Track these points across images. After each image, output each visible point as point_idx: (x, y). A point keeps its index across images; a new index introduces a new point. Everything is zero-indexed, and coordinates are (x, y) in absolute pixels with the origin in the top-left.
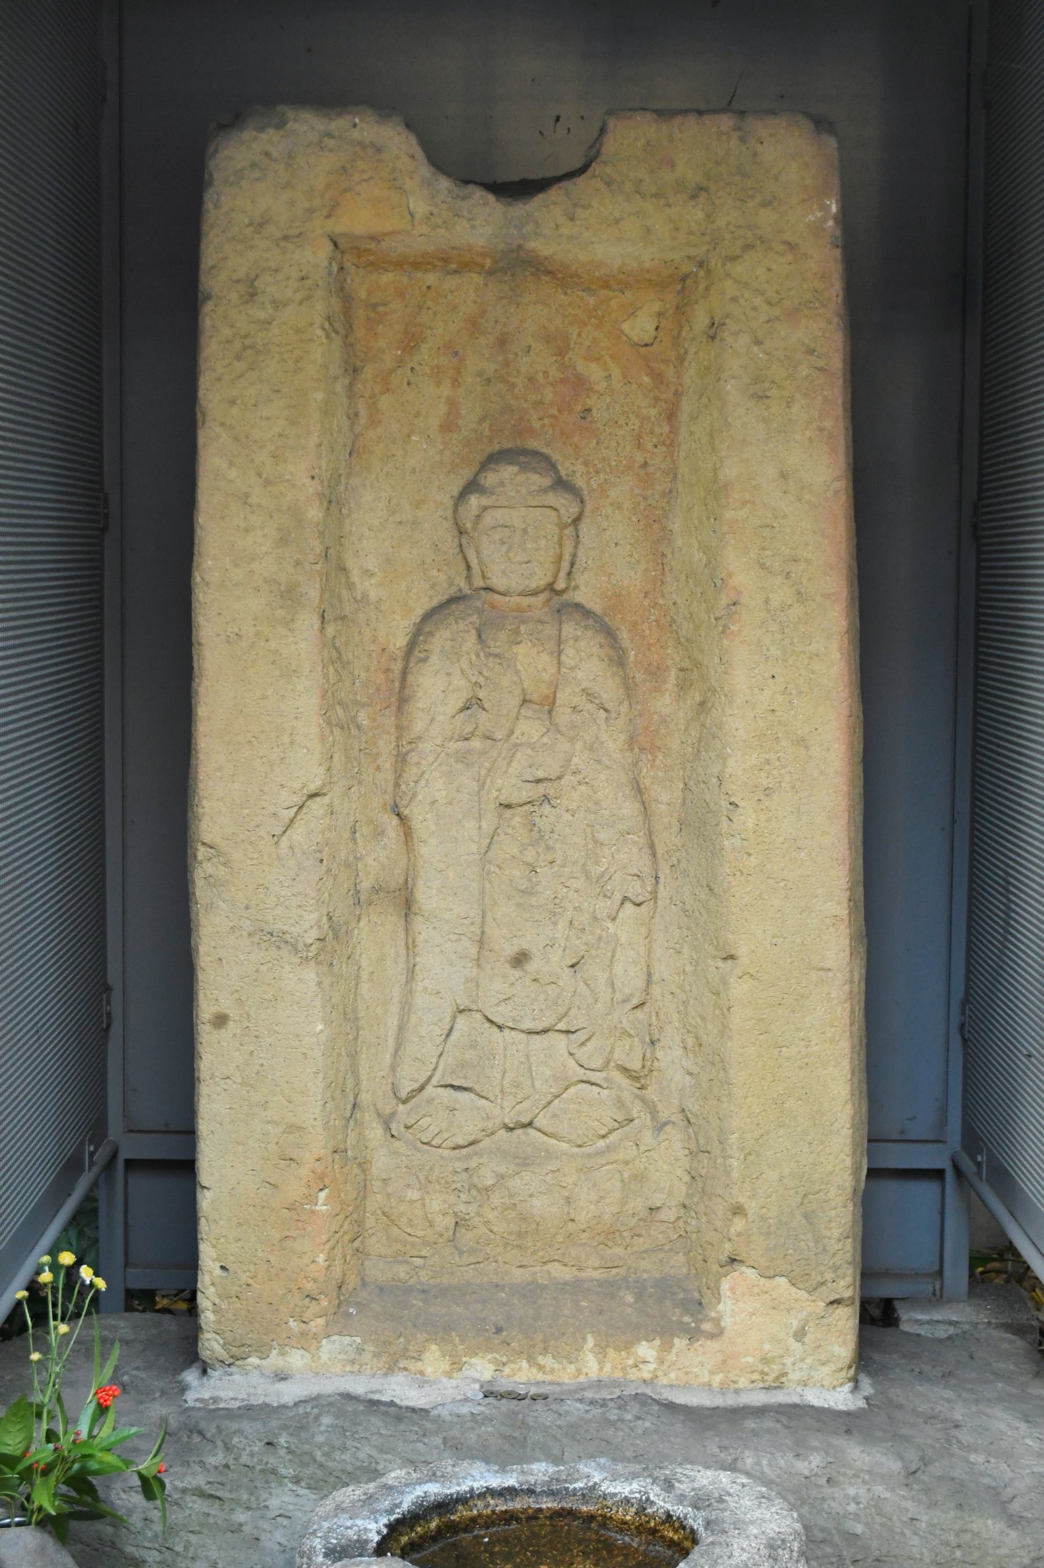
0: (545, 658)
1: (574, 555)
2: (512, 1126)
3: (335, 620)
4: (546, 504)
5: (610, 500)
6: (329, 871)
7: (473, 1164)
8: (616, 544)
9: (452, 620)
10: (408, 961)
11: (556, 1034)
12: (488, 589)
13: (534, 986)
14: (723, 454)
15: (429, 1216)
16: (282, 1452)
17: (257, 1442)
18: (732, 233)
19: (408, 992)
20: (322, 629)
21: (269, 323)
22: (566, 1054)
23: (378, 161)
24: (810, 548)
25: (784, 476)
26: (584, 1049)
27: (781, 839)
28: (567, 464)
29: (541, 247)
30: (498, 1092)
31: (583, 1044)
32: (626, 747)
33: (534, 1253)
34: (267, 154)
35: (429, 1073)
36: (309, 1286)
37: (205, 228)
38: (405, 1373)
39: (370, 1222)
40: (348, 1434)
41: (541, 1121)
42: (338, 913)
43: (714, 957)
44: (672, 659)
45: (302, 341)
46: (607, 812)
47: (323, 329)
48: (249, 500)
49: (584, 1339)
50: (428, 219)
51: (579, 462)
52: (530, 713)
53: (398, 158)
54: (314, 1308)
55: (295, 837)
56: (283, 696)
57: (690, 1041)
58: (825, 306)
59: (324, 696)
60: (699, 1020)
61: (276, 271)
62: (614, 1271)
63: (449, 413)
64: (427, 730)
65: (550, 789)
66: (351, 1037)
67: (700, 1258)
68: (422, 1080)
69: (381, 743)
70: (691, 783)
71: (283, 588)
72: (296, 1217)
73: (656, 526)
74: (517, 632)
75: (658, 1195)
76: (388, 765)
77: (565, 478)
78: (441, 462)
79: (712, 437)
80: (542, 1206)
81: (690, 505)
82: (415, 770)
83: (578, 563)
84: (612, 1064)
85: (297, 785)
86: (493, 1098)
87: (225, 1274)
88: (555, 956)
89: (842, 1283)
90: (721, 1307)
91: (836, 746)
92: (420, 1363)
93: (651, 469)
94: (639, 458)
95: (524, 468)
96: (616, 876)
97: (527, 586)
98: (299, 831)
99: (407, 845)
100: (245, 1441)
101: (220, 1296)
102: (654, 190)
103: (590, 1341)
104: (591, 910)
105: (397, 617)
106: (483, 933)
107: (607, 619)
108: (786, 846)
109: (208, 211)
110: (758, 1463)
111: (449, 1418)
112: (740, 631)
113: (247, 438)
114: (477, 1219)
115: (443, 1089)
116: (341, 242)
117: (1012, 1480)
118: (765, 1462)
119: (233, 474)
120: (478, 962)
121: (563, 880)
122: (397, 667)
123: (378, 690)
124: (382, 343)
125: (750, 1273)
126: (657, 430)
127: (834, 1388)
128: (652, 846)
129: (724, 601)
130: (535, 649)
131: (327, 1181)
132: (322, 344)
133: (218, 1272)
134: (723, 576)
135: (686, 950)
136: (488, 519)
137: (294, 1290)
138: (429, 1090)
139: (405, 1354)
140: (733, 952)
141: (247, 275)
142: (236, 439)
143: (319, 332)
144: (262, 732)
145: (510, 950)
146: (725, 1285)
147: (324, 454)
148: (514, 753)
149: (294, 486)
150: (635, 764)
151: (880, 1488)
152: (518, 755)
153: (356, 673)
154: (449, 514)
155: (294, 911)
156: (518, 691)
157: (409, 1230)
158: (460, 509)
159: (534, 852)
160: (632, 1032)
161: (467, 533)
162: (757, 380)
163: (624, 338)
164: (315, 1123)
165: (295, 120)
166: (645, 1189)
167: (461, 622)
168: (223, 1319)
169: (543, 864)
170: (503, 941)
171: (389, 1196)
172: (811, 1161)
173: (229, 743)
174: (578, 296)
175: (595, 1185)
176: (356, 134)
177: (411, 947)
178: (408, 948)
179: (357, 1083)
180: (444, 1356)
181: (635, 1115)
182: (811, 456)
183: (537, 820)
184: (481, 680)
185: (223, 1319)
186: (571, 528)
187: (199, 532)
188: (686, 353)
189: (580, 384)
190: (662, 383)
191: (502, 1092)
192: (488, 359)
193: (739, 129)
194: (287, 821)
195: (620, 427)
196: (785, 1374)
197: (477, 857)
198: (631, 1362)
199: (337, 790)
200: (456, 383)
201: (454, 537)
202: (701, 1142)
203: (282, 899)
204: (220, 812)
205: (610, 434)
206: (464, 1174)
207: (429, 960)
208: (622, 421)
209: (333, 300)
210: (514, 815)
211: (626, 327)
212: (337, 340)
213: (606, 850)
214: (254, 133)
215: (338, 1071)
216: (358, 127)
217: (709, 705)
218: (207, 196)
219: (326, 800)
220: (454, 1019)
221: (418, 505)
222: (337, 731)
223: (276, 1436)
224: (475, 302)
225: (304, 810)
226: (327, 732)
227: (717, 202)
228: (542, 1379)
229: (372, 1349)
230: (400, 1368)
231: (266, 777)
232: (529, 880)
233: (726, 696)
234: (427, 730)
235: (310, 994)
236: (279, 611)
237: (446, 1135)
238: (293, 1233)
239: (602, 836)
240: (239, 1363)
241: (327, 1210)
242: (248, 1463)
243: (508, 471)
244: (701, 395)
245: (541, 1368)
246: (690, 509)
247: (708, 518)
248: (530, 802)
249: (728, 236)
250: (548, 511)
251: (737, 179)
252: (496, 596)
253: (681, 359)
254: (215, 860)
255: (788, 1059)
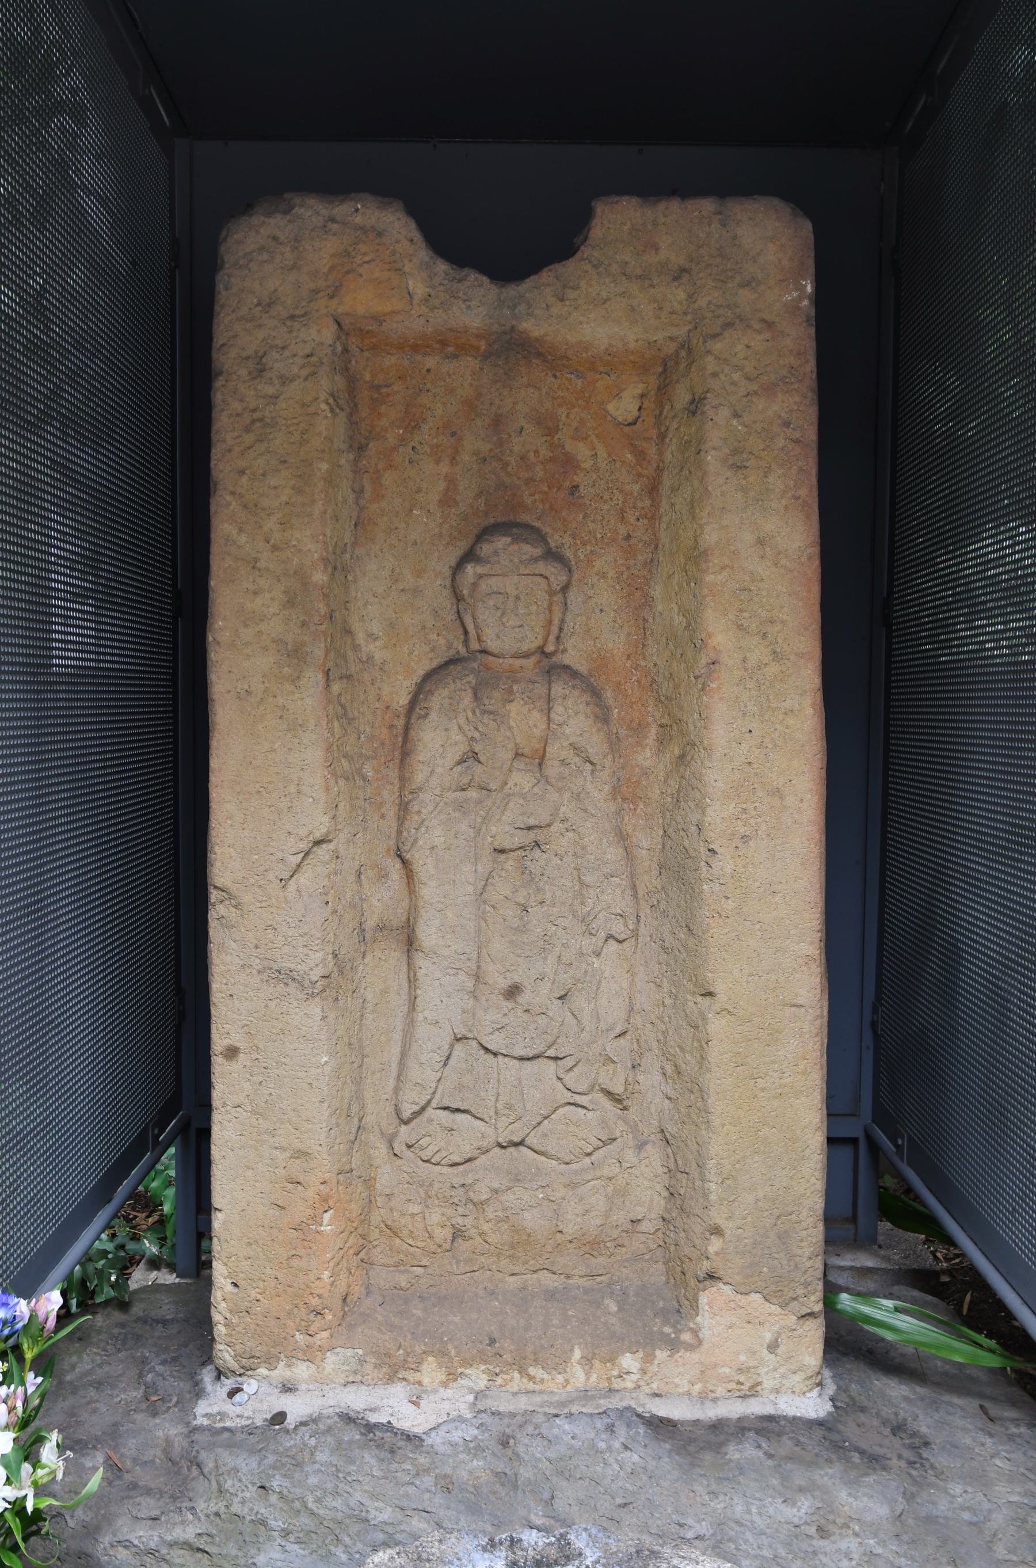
0: (536, 714)
1: (563, 621)
2: (505, 1144)
3: (341, 678)
4: (537, 572)
5: (595, 570)
6: (334, 912)
7: (469, 1181)
8: (601, 610)
9: (450, 679)
10: (410, 993)
11: (546, 1060)
12: (484, 652)
13: (525, 1017)
14: (704, 521)
15: (429, 1228)
16: (274, 1498)
17: (250, 1486)
18: (713, 312)
19: (410, 1023)
20: (328, 686)
21: (277, 398)
22: (555, 1078)
23: (379, 245)
24: (786, 609)
25: (761, 542)
26: (571, 1074)
27: (757, 884)
28: (556, 537)
29: (532, 327)
30: (492, 1112)
31: (570, 1069)
32: (610, 797)
33: (525, 1263)
34: (275, 238)
35: (429, 1097)
36: (314, 1302)
37: (217, 308)
38: (404, 1383)
39: (375, 1234)
40: (341, 1475)
41: (530, 1141)
42: (343, 951)
43: (693, 993)
44: (653, 716)
45: (307, 415)
46: (592, 857)
47: (328, 404)
48: (258, 565)
49: (572, 1350)
50: (427, 300)
51: (566, 536)
52: (522, 766)
53: (398, 242)
54: (318, 1323)
55: (302, 880)
56: (290, 749)
57: (669, 1069)
58: (800, 381)
59: (328, 749)
60: (677, 1049)
61: (283, 348)
62: (599, 1279)
63: (447, 489)
64: (427, 781)
65: (540, 835)
66: (356, 1065)
67: (679, 1269)
68: (423, 1103)
69: (385, 793)
70: (671, 831)
71: (290, 647)
72: (303, 1237)
73: (638, 594)
74: (510, 691)
75: (639, 1208)
76: (392, 813)
77: (554, 550)
78: (441, 535)
79: (693, 507)
80: (530, 1219)
81: (671, 572)
82: (416, 817)
83: (565, 628)
84: (597, 1087)
85: (303, 832)
86: (487, 1119)
87: (236, 1290)
88: (545, 988)
89: (813, 1298)
90: (699, 1319)
91: (809, 796)
92: (418, 1374)
93: (633, 541)
94: (623, 531)
95: (516, 540)
96: (601, 915)
97: (519, 648)
98: (306, 875)
99: (409, 887)
100: (238, 1484)
101: (231, 1311)
102: (639, 272)
103: (577, 1354)
104: (578, 946)
105: (400, 677)
106: (479, 967)
107: (592, 680)
108: (762, 890)
109: (219, 293)
110: (748, 1512)
111: (441, 1449)
112: (719, 688)
113: (256, 506)
114: (473, 1231)
115: (441, 1111)
116: (346, 322)
117: (990, 1511)
118: (754, 1510)
119: (243, 539)
120: (474, 995)
121: (551, 918)
122: (400, 723)
123: (382, 744)
124: (384, 422)
125: (727, 1289)
126: (639, 504)
127: (804, 1393)
128: (634, 887)
129: (704, 661)
130: (527, 707)
131: (331, 1203)
132: (327, 417)
133: (230, 1288)
134: (703, 636)
135: (665, 984)
136: (484, 587)
137: (301, 1305)
138: (430, 1112)
139: (404, 1365)
140: (712, 989)
141: (256, 352)
142: (245, 507)
143: (323, 406)
144: (270, 782)
145: (503, 983)
146: (704, 1299)
147: (329, 522)
148: (508, 803)
149: (300, 551)
150: (618, 812)
151: (872, 1542)
152: (511, 804)
153: (362, 728)
154: (448, 582)
155: (301, 950)
156: (511, 746)
157: (410, 1241)
158: (457, 577)
159: (525, 893)
160: (615, 1059)
161: (464, 600)
162: (736, 451)
163: (609, 418)
164: (319, 1148)
165: (301, 206)
166: (627, 1203)
167: (458, 682)
168: (234, 1333)
169: (533, 904)
170: (497, 974)
171: (391, 1210)
172: (785, 1185)
173: (239, 793)
174: (567, 378)
175: (581, 1199)
176: (358, 219)
177: (412, 981)
178: (410, 982)
179: (363, 1107)
180: (440, 1368)
181: (618, 1135)
182: (787, 523)
183: (528, 863)
184: (477, 735)
185: (234, 1333)
186: (560, 595)
187: (212, 595)
188: (667, 429)
189: (569, 462)
190: (644, 459)
191: (496, 1113)
192: (483, 439)
193: (720, 213)
194: (294, 866)
195: (606, 502)
196: (759, 1384)
197: (473, 898)
198: (615, 1373)
199: (342, 837)
200: (453, 461)
201: (452, 604)
202: (680, 1163)
203: (290, 939)
204: (231, 857)
205: (596, 508)
206: (462, 1189)
207: (430, 995)
208: (606, 496)
209: (337, 378)
210: (507, 859)
211: (610, 407)
212: (342, 418)
213: (591, 891)
214: (262, 218)
215: (342, 1099)
216: (361, 212)
217: (689, 758)
218: (218, 277)
219: (331, 846)
220: (452, 1047)
221: (419, 574)
222: (342, 782)
223: (270, 1477)
224: (471, 385)
225: (311, 856)
226: (332, 782)
227: (699, 283)
228: (531, 1389)
229: (373, 1360)
230: (399, 1379)
231: (274, 824)
232: (522, 918)
233: (705, 749)
234: (427, 781)
235: (315, 1028)
236: (286, 669)
237: (444, 1154)
238: (302, 1252)
239: (588, 879)
240: (249, 1373)
241: (332, 1230)
242: (239, 1512)
243: (502, 542)
244: (682, 468)
245: (531, 1378)
246: (670, 577)
247: (688, 584)
248: (521, 848)
249: (709, 315)
250: (539, 579)
251: (718, 260)
252: (491, 658)
253: (662, 437)
254: (227, 902)
255: (763, 1090)
